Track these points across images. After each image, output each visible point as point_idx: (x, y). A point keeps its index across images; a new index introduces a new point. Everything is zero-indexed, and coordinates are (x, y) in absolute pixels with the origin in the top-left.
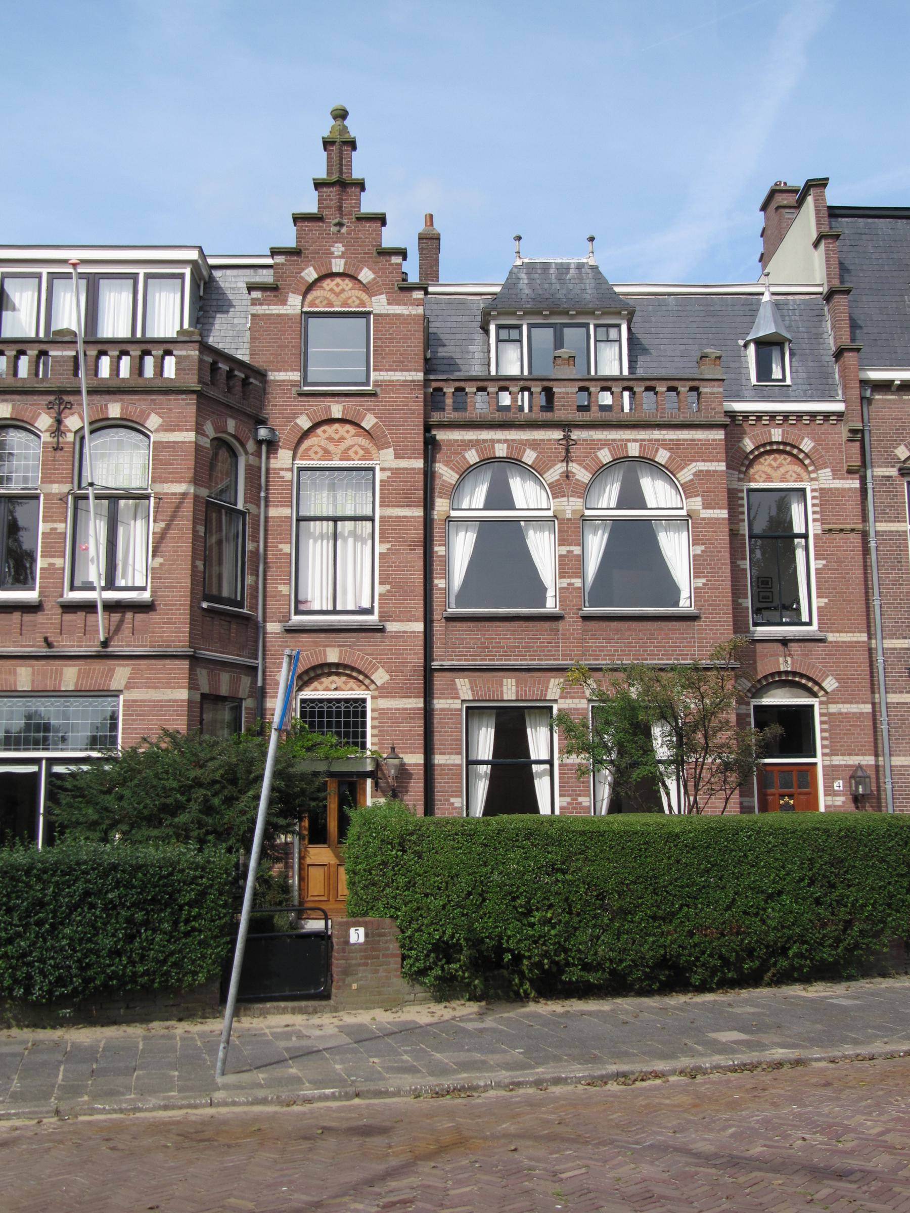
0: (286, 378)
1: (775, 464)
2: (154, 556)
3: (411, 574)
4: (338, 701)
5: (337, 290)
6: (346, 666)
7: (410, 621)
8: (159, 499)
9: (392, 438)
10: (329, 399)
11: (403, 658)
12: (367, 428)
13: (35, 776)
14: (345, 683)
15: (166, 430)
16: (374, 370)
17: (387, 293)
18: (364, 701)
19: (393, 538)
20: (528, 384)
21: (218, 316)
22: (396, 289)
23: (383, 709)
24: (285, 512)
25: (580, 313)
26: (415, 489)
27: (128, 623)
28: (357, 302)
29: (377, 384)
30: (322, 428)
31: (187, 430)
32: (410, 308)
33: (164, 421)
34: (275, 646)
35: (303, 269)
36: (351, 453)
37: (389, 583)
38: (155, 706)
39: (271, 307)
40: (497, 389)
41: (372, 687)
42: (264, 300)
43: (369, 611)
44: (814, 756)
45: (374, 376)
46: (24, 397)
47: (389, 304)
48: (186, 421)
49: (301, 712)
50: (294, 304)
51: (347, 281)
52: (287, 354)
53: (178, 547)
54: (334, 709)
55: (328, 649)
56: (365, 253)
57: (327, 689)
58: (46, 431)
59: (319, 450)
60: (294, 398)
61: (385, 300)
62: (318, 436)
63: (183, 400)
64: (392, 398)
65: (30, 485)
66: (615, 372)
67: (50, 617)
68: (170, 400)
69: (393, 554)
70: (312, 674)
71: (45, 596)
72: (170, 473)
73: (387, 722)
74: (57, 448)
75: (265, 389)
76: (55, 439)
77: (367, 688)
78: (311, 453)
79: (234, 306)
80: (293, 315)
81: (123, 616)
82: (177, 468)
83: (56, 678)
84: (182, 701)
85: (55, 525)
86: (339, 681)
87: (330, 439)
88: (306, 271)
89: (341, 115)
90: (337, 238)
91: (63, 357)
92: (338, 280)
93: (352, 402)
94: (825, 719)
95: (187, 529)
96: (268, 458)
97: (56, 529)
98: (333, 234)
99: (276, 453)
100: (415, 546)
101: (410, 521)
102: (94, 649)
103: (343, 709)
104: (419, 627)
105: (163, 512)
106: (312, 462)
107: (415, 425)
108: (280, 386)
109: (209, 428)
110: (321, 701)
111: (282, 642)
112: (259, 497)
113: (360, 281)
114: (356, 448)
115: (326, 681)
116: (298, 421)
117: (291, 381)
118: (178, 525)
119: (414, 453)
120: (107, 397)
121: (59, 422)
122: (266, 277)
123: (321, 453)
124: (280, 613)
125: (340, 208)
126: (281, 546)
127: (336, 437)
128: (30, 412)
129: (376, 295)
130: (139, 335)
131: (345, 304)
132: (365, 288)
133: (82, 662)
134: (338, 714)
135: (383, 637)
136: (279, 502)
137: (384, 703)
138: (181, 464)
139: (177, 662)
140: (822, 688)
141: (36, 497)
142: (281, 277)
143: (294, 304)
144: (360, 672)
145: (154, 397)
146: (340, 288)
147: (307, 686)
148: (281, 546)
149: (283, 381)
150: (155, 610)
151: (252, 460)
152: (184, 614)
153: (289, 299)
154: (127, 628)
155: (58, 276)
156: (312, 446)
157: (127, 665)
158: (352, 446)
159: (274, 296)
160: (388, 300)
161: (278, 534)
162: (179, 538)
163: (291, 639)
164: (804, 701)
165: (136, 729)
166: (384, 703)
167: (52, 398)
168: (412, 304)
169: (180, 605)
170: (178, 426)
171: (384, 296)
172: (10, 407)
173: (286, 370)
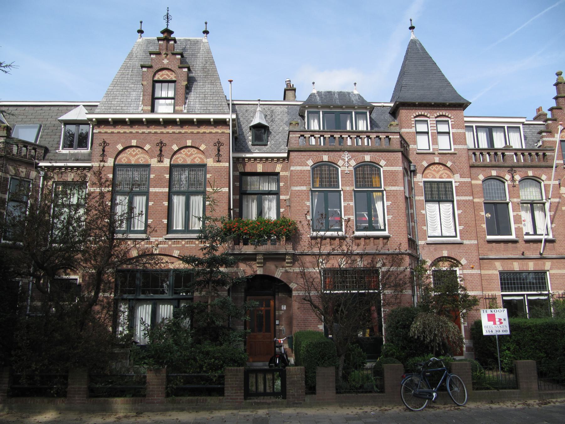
1: (437, 170)
13: (522, 301)
25: (347, 107)
30: (183, 150)
46: (500, 169)
66: (317, 128)
67: (521, 245)
74: (514, 186)
87: (186, 154)
89: (559, 74)
102: (539, 256)
114: (445, 174)
120: (527, 169)
121: (513, 177)
130: (477, 147)
141: (507, 204)
167: (509, 169)
172: (495, 171)
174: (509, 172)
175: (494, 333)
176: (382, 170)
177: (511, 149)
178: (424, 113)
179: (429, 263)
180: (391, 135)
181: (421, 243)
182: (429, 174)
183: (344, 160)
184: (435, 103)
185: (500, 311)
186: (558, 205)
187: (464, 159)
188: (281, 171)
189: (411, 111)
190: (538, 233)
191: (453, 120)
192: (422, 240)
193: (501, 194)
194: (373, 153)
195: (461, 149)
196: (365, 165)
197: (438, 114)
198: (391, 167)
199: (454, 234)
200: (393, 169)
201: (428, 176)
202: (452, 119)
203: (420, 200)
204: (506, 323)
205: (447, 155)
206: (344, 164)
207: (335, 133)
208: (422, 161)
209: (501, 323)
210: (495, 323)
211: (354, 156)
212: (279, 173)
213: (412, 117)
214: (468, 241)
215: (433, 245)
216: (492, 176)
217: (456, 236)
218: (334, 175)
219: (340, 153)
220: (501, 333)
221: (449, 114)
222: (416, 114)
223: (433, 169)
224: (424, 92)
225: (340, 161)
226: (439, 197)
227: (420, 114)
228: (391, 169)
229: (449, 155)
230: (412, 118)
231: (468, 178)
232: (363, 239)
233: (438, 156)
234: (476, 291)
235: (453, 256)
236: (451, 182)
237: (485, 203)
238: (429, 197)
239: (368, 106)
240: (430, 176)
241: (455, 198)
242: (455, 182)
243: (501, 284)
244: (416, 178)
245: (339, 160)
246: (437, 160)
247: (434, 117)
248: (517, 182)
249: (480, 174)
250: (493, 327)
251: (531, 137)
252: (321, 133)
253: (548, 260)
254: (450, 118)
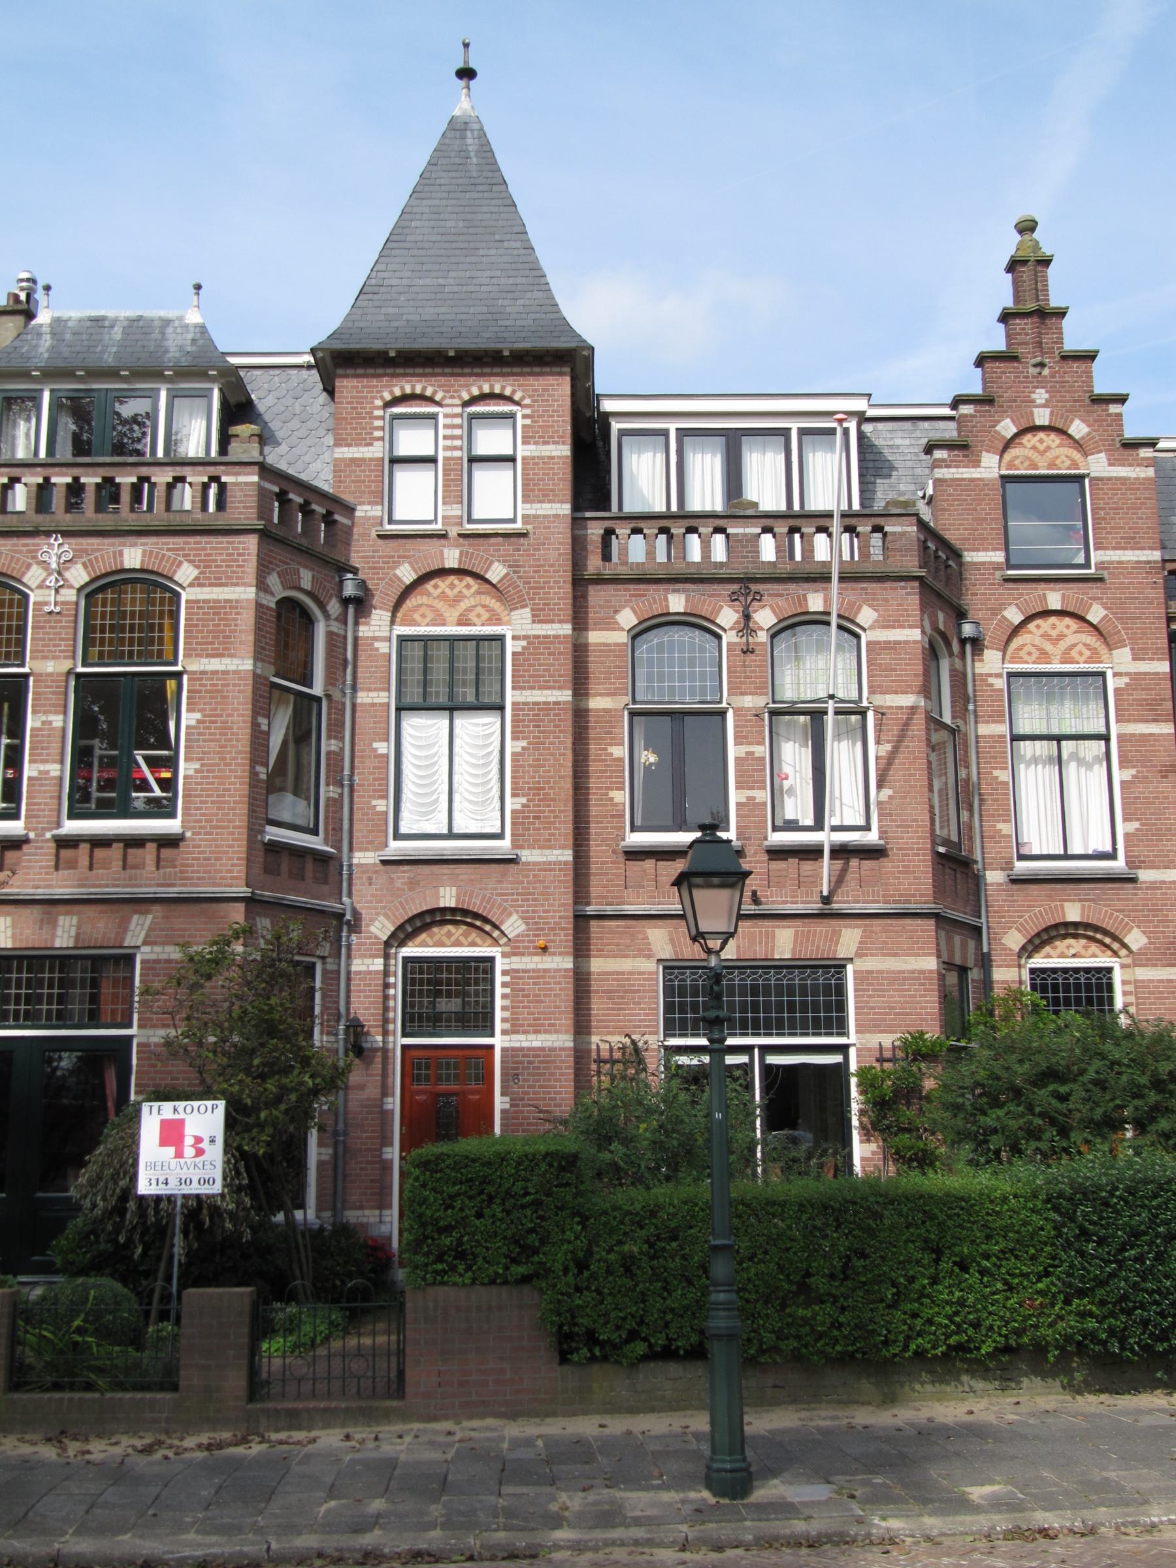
0: (987, 559)
1: (450, 593)
2: (880, 786)
3: (1165, 808)
4: (1076, 970)
5: (1041, 447)
6: (465, 912)
7: (1168, 867)
8: (881, 713)
9: (1127, 634)
10: (1043, 585)
11: (1163, 915)
12: (1095, 622)
14: (466, 935)
15: (884, 627)
16: (1096, 549)
17: (1106, 451)
18: (1109, 970)
19: (1138, 761)
21: (878, 481)
22: (1118, 445)
23: (1143, 981)
24: (380, 697)
26: (1162, 700)
27: (854, 872)
28: (1068, 463)
29: (1101, 566)
30: (433, 582)
31: (910, 627)
32: (1138, 469)
33: (880, 616)
34: (997, 901)
35: (999, 422)
36: (1074, 653)
37: (1137, 820)
38: (896, 979)
39: (961, 470)
40: (683, 530)
41: (503, 941)
42: (951, 461)
43: (1112, 856)
44: (492, 1035)
45: (1095, 557)
46: (701, 586)
47: (1110, 465)
48: (908, 616)
49: (1031, 984)
50: (990, 467)
51: (1053, 436)
52: (985, 529)
53: (911, 775)
54: (1071, 981)
55: (1066, 904)
56: (1075, 401)
57: (1062, 956)
58: (732, 629)
59: (1033, 650)
60: (999, 584)
61: (1105, 460)
62: (1030, 632)
63: (903, 588)
64: (1123, 583)
65: (677, 699)
68: (885, 589)
69: (1140, 782)
70: (1045, 937)
71: (746, 839)
72: (894, 681)
73: (1149, 998)
74: (747, 651)
75: (961, 574)
76: (744, 639)
77: (496, 942)
78: (1022, 653)
79: (896, 469)
80: (990, 480)
81: (847, 864)
82: (901, 675)
83: (767, 943)
84: (930, 971)
85: (752, 748)
86: (1077, 945)
87: (1045, 636)
88: (1002, 424)
89: (1027, 227)
90: (1038, 382)
91: (745, 535)
92: (1041, 435)
93: (1073, 589)
94: (1130, 988)
95: (919, 752)
96: (356, 623)
97: (752, 753)
98: (1033, 377)
99: (982, 655)
100: (1167, 771)
101: (1158, 740)
102: (815, 906)
103: (1060, 981)
104: (567, 855)
105: (888, 731)
106: (1026, 666)
107: (1155, 618)
108: (979, 569)
109: (273, 580)
110: (1054, 970)
111: (1007, 895)
112: (966, 710)
113: (1070, 436)
114: (480, 610)
115: (1061, 945)
116: (1006, 613)
117: (993, 563)
118: (908, 747)
119: (1156, 654)
120: (806, 585)
121: (747, 617)
122: (949, 431)
123: (1036, 654)
124: (1003, 858)
125: (1039, 344)
126: (996, 773)
127: (1054, 633)
128: (709, 605)
129: (1093, 454)
130: (796, 507)
131: (1051, 465)
132: (1078, 444)
133: (799, 922)
134: (1078, 988)
135: (1135, 889)
136: (989, 716)
137: (518, 963)
138: (906, 670)
139: (919, 922)
140: (1124, 946)
141: (722, 714)
142: (971, 432)
143: (990, 467)
144: (1115, 938)
145: (865, 585)
146: (1045, 445)
147: (1037, 952)
148: (996, 773)
149: (983, 563)
150: (887, 856)
151: (335, 627)
152: (924, 861)
153: (983, 460)
154: (853, 879)
155: (689, 433)
156: (1025, 645)
157: (857, 926)
158: (1075, 645)
159: (964, 456)
160: (1109, 460)
161: (991, 758)
162: (910, 764)
163: (1018, 892)
164: (1102, 960)
165: (874, 1008)
166: (518, 963)
167: (736, 587)
168: (1139, 465)
169: (919, 849)
170: (898, 621)
171: (1103, 455)
172: (683, 597)
173: (986, 550)
174: (734, 598)
175: (173, 1189)
176: (184, 598)
177: (750, 512)
178: (424, 389)
179: (380, 928)
180: (228, 474)
181: (363, 861)
182: (423, 610)
183: (44, 564)
184: (400, 353)
185: (202, 1109)
186: (909, 719)
187: (553, 555)
189: (374, 382)
191: (528, 411)
192: (367, 850)
193: (704, 679)
194: (154, 539)
195: (545, 516)
196: (125, 581)
197: (398, 392)
198: (215, 589)
200: (222, 597)
201: (417, 616)
202: (527, 406)
203: (373, 705)
204: (215, 1154)
205: (493, 540)
206: (44, 581)
207: (25, 470)
208: (397, 564)
209: (200, 1152)
210: (179, 1154)
211: (85, 551)
213: (379, 403)
214: (536, 852)
215: (406, 868)
216: (668, 614)
218: (103, 618)
219: (37, 541)
220: (194, 1189)
221: (514, 392)
222: (391, 392)
223: (436, 593)
224: (437, 310)
225: (34, 568)
226: (451, 696)
227: (408, 391)
228: (214, 596)
229: (500, 539)
230: (377, 408)
231: (560, 622)
232: (151, 847)
233: (457, 546)
234: (547, 1032)
235: (475, 905)
236: (500, 639)
237: (633, 714)
238: (414, 695)
239: (213, 368)
240: (423, 616)
241: (510, 697)
242: (514, 638)
243: (669, 1008)
244: (367, 624)
245: (29, 567)
246: (452, 558)
247: (458, 402)
248: (763, 637)
249: (623, 607)
250: (172, 1166)
251: (909, 464)
252: (212, 470)
253: (785, 923)
254: (517, 403)
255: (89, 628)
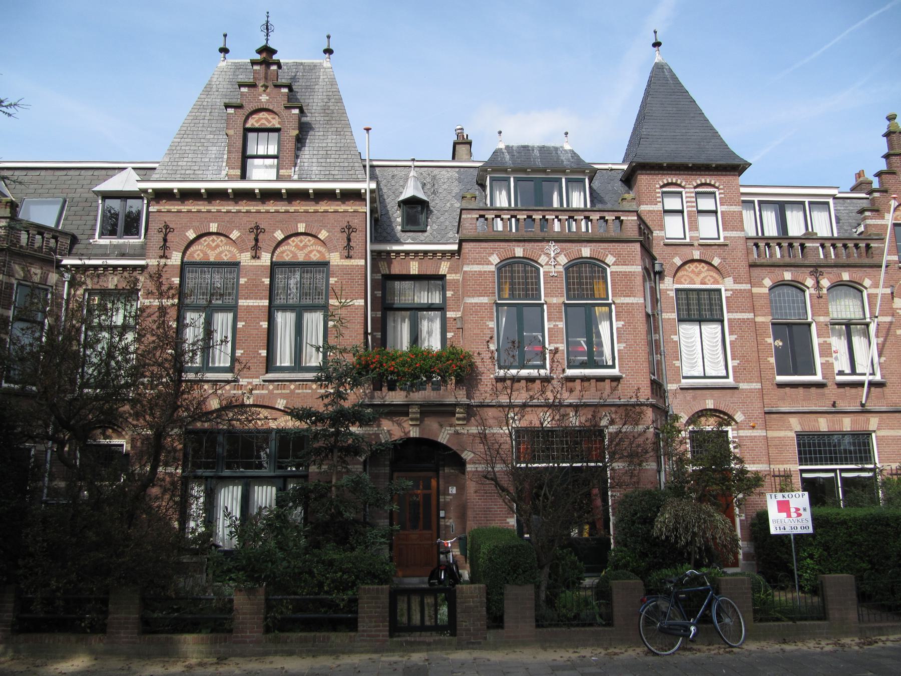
1: (696, 270)
20: (515, 213)
25: (554, 171)
40: (509, 217)
46: (797, 269)
74: (820, 297)
87: (296, 246)
102: (859, 408)
114: (709, 277)
120: (841, 269)
121: (818, 282)
130: (760, 234)
141: (809, 325)
167: (812, 269)
172: (790, 273)
174: (811, 274)
175: (788, 531)
176: (609, 270)
177: (815, 237)
178: (677, 180)
180: (623, 216)
181: (672, 388)
182: (685, 277)
183: (548, 255)
184: (694, 165)
185: (797, 496)
186: (890, 327)
187: (740, 254)
188: (448, 273)
189: (655, 177)
190: (857, 372)
191: (722, 191)
192: (673, 383)
193: (799, 309)
194: (595, 244)
195: (735, 237)
196: (581, 263)
197: (699, 182)
198: (624, 267)
199: (724, 373)
200: (627, 270)
201: (682, 280)
202: (721, 189)
203: (669, 319)
204: (807, 515)
205: (713, 247)
206: (548, 262)
207: (534, 212)
208: (673, 257)
209: (799, 515)
210: (789, 516)
211: (565, 249)
212: (445, 276)
213: (658, 186)
214: (746, 384)
215: (691, 391)
216: (784, 281)
217: (727, 377)
219: (542, 244)
220: (799, 531)
221: (715, 183)
222: (663, 182)
223: (690, 270)
224: (677, 146)
225: (543, 256)
226: (700, 315)
227: (670, 181)
228: (623, 270)
229: (716, 247)
230: (657, 188)
231: (746, 283)
232: (578, 381)
233: (699, 249)
234: (758, 463)
235: (722, 408)
236: (719, 291)
237: (773, 324)
238: (684, 314)
239: (587, 169)
240: (685, 280)
241: (726, 316)
242: (726, 290)
243: (800, 453)
244: (663, 283)
245: (540, 256)
246: (696, 255)
247: (691, 186)
248: (825, 291)
249: (765, 277)
250: (786, 521)
251: (846, 218)
252: (512, 213)
253: (874, 415)
254: (717, 188)
255: (568, 284)
